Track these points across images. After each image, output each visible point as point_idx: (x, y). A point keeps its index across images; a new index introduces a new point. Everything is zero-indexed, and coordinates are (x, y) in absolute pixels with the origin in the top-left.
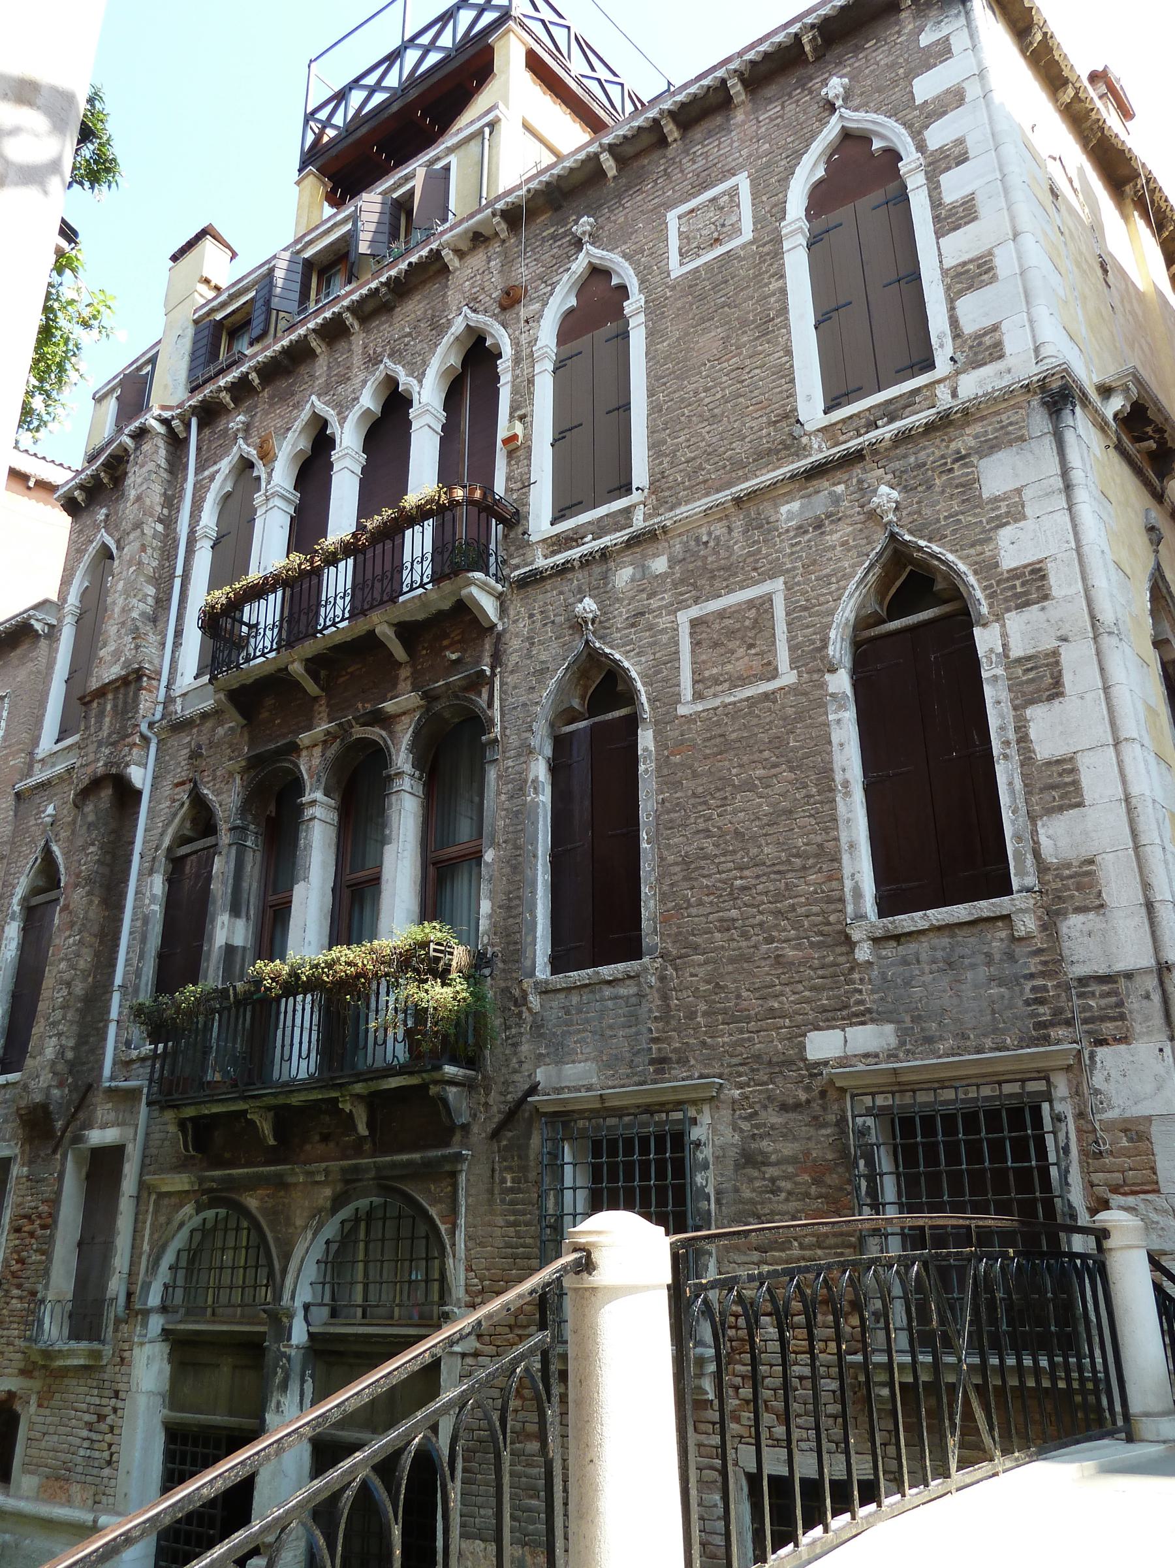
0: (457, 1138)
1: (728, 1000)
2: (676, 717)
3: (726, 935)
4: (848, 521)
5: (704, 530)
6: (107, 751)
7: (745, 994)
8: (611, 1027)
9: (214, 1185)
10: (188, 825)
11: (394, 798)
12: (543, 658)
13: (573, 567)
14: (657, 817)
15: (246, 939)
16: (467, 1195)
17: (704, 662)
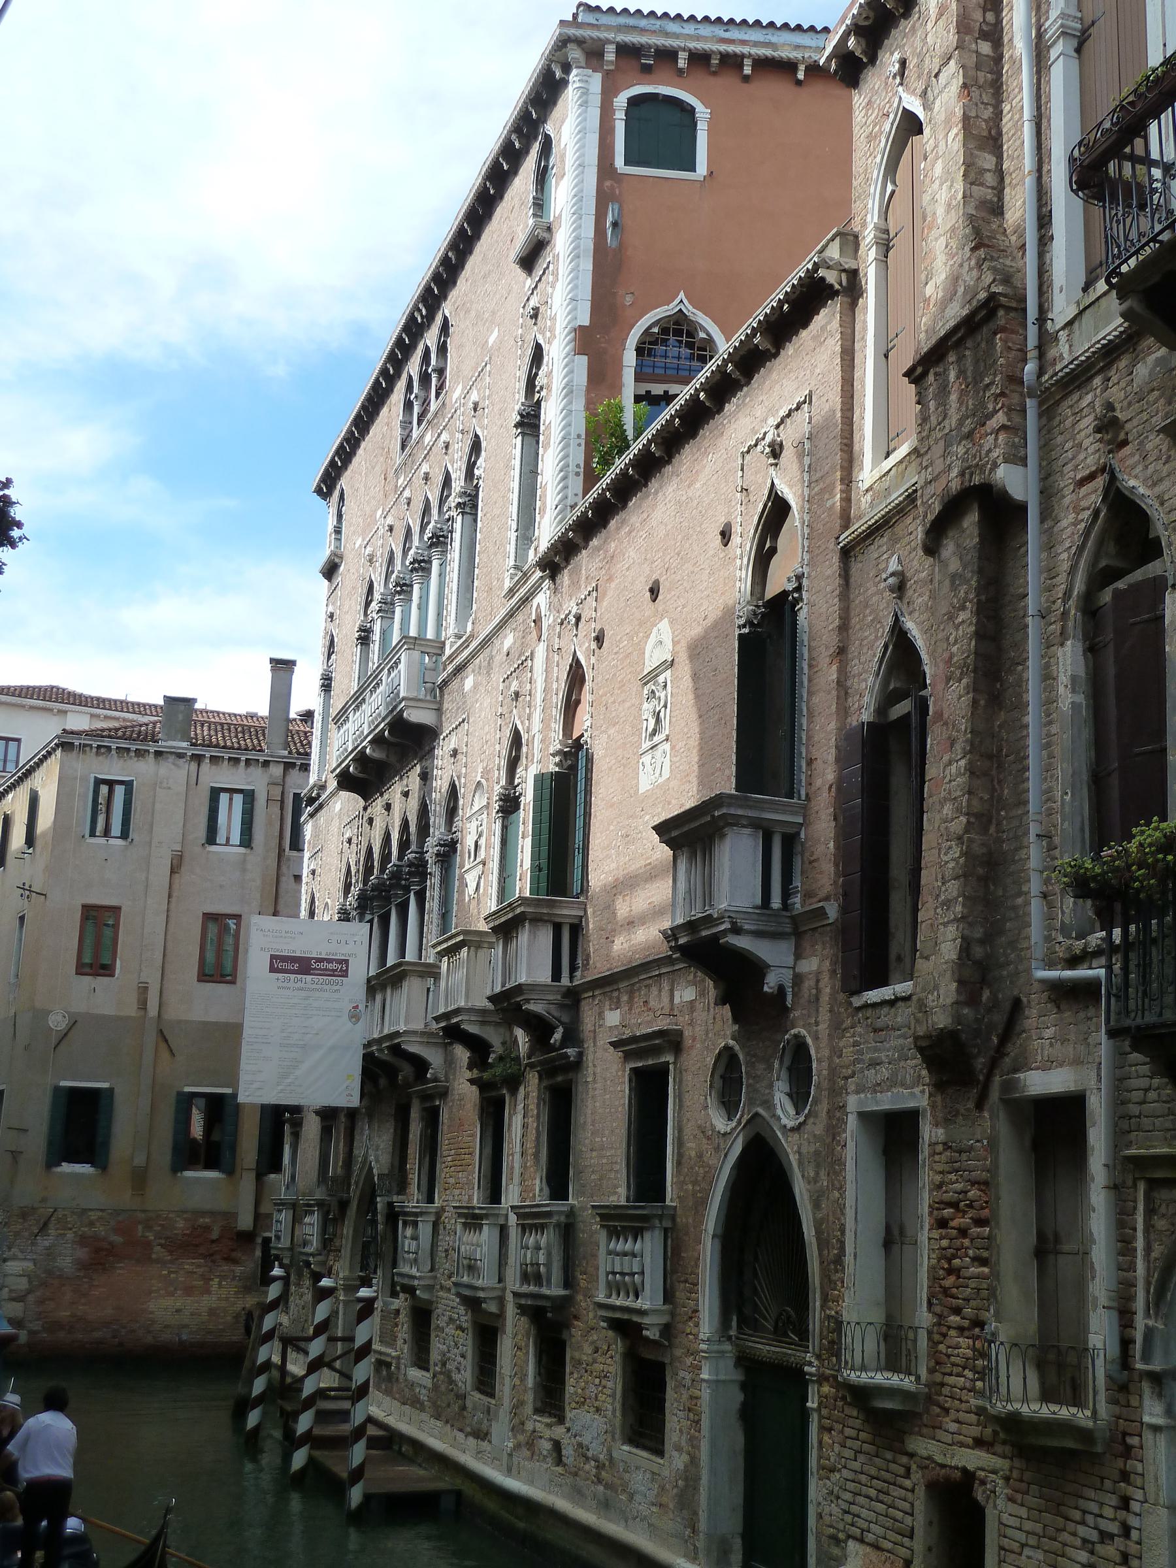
6: (961, 450)
10: (1111, 548)
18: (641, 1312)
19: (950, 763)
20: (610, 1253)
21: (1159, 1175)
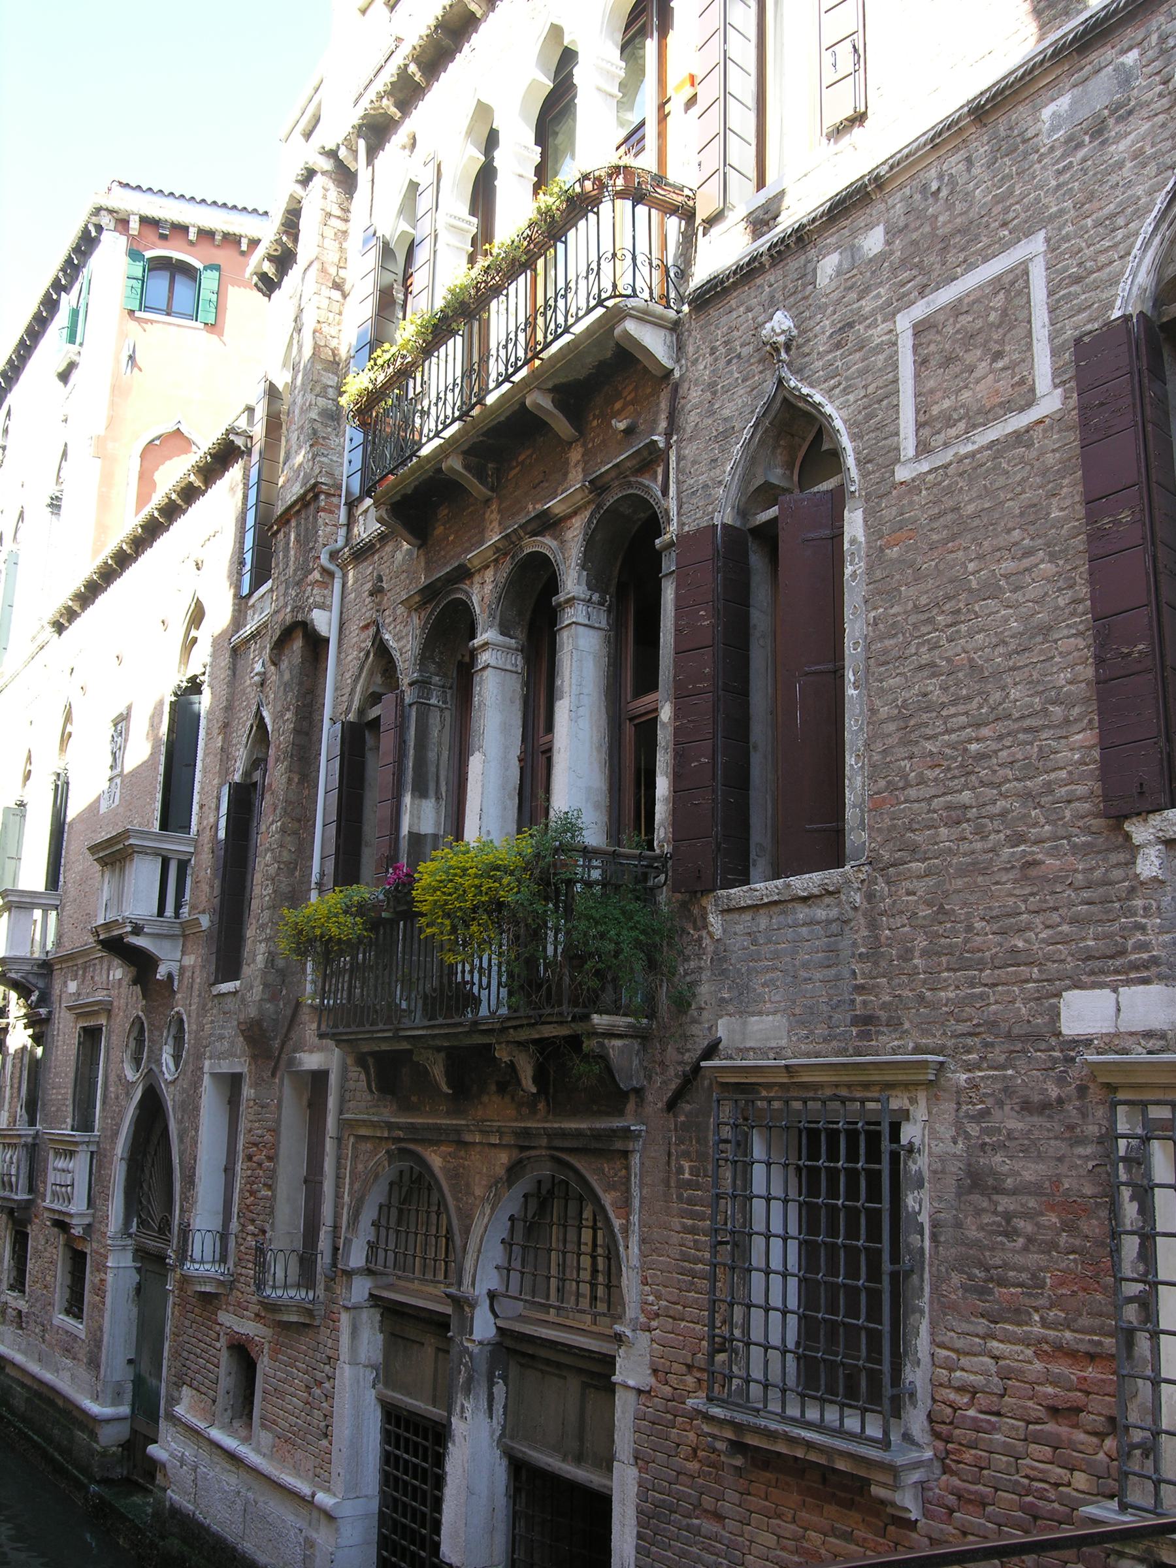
0: (631, 1106)
1: (954, 932)
2: (894, 486)
3: (956, 832)
4: (1145, 113)
5: (933, 173)
6: (294, 594)
7: (978, 925)
8: (805, 965)
9: (401, 1134)
11: (565, 634)
12: (726, 413)
13: (762, 265)
14: (868, 647)
15: (437, 824)
16: (642, 1186)
17: (932, 392)
18: (71, 1215)
19: (272, 824)
20: (55, 1169)
21: (363, 1132)
